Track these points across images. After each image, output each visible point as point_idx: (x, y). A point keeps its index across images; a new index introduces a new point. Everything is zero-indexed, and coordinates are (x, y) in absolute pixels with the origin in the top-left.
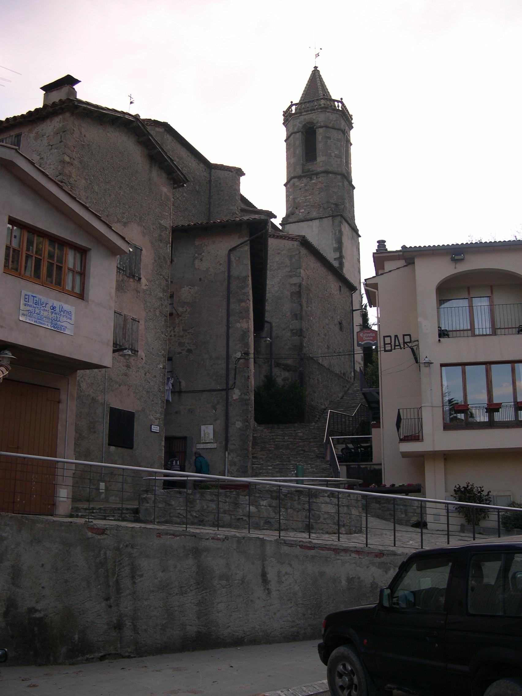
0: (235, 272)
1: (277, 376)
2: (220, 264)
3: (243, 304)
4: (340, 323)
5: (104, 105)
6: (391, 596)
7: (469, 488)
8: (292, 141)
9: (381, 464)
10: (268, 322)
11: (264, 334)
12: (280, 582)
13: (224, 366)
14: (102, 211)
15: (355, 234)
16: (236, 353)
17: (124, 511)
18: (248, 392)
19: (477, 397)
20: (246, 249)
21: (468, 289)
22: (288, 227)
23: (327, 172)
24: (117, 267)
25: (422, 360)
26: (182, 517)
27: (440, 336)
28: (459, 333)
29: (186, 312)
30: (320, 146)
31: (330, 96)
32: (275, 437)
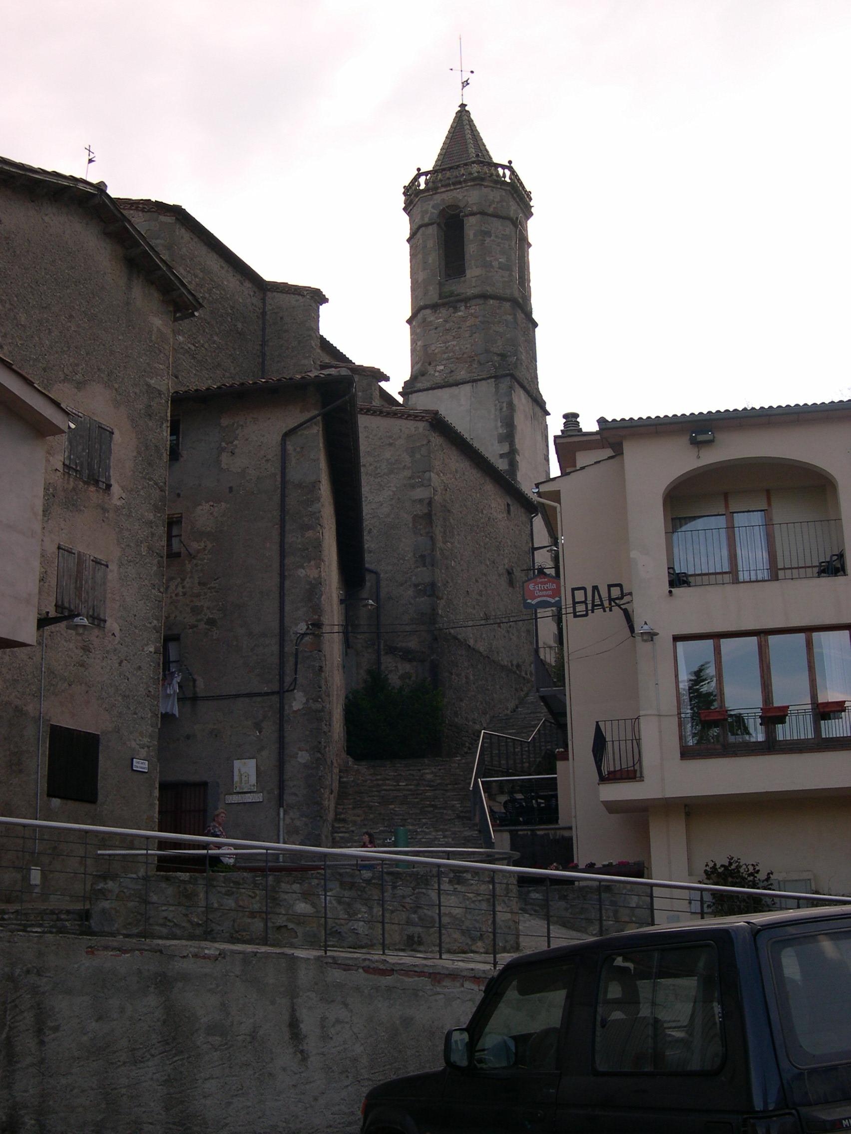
0: (294, 475)
1: (391, 671)
2: (267, 461)
3: (310, 534)
4: (510, 573)
5: (36, 165)
6: (472, 1046)
7: (733, 867)
8: (421, 241)
9: (570, 828)
10: (371, 571)
11: (365, 594)
12: (325, 1037)
13: (275, 649)
14: (35, 360)
15: (537, 409)
16: (297, 625)
17: (63, 917)
18: (320, 697)
19: (741, 697)
20: (315, 431)
21: (726, 496)
22: (414, 398)
23: (484, 297)
24: (64, 464)
25: (638, 630)
26: (171, 924)
27: (672, 584)
28: (707, 578)
29: (204, 549)
30: (471, 249)
31: (491, 158)
32: (380, 782)
